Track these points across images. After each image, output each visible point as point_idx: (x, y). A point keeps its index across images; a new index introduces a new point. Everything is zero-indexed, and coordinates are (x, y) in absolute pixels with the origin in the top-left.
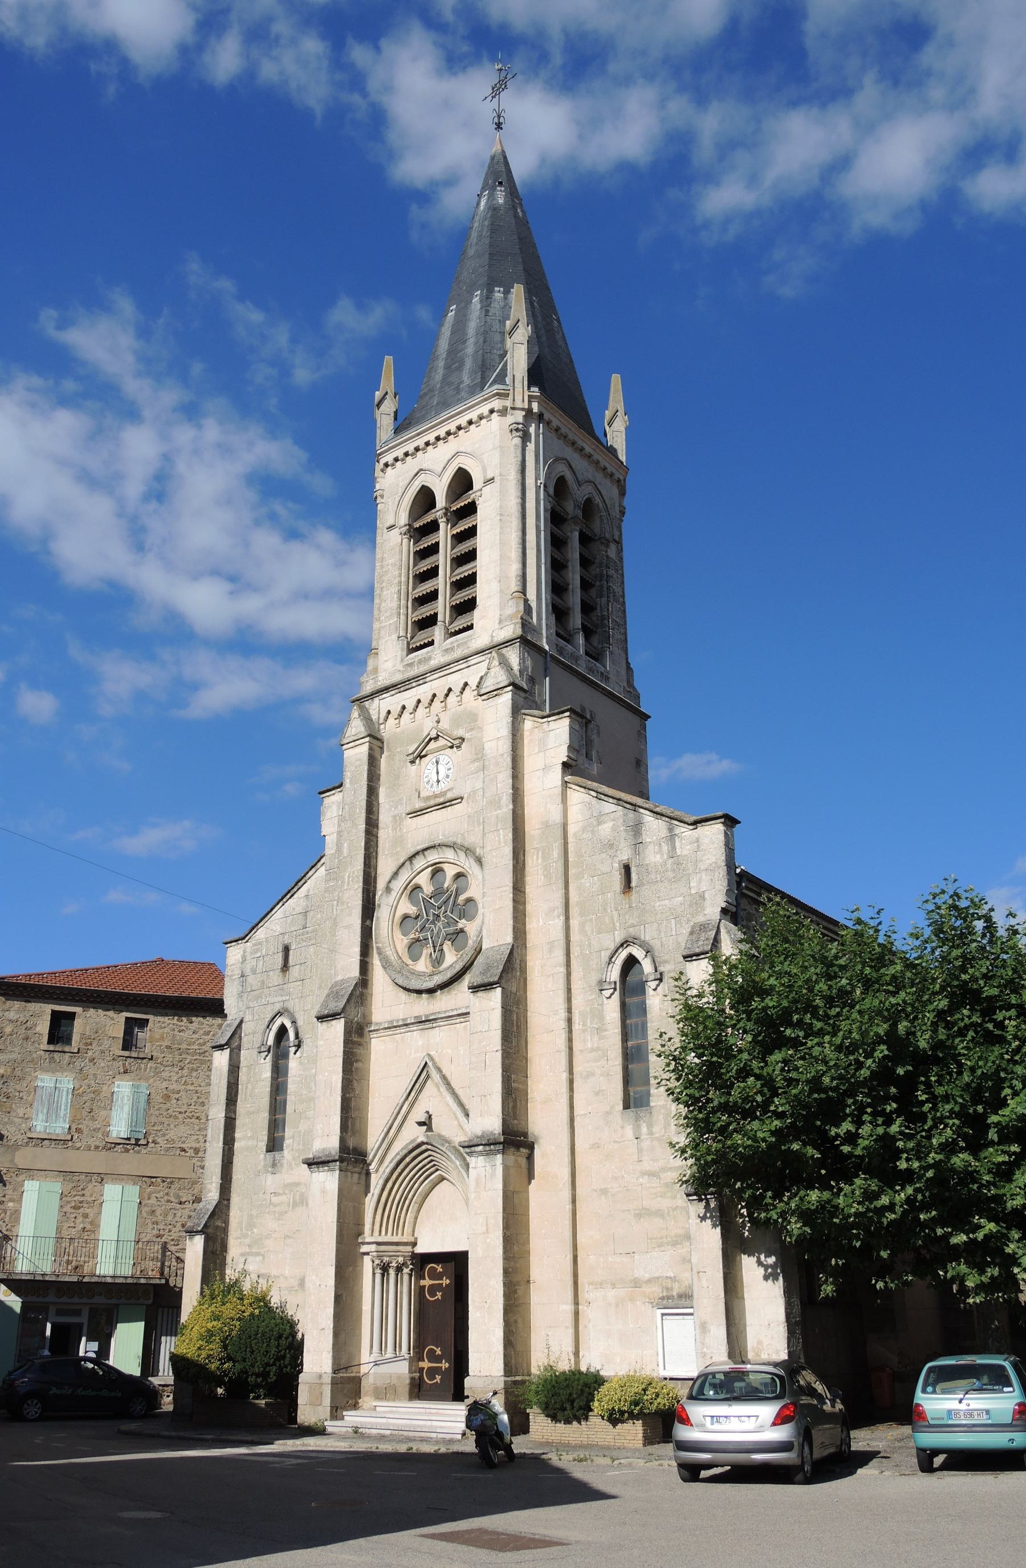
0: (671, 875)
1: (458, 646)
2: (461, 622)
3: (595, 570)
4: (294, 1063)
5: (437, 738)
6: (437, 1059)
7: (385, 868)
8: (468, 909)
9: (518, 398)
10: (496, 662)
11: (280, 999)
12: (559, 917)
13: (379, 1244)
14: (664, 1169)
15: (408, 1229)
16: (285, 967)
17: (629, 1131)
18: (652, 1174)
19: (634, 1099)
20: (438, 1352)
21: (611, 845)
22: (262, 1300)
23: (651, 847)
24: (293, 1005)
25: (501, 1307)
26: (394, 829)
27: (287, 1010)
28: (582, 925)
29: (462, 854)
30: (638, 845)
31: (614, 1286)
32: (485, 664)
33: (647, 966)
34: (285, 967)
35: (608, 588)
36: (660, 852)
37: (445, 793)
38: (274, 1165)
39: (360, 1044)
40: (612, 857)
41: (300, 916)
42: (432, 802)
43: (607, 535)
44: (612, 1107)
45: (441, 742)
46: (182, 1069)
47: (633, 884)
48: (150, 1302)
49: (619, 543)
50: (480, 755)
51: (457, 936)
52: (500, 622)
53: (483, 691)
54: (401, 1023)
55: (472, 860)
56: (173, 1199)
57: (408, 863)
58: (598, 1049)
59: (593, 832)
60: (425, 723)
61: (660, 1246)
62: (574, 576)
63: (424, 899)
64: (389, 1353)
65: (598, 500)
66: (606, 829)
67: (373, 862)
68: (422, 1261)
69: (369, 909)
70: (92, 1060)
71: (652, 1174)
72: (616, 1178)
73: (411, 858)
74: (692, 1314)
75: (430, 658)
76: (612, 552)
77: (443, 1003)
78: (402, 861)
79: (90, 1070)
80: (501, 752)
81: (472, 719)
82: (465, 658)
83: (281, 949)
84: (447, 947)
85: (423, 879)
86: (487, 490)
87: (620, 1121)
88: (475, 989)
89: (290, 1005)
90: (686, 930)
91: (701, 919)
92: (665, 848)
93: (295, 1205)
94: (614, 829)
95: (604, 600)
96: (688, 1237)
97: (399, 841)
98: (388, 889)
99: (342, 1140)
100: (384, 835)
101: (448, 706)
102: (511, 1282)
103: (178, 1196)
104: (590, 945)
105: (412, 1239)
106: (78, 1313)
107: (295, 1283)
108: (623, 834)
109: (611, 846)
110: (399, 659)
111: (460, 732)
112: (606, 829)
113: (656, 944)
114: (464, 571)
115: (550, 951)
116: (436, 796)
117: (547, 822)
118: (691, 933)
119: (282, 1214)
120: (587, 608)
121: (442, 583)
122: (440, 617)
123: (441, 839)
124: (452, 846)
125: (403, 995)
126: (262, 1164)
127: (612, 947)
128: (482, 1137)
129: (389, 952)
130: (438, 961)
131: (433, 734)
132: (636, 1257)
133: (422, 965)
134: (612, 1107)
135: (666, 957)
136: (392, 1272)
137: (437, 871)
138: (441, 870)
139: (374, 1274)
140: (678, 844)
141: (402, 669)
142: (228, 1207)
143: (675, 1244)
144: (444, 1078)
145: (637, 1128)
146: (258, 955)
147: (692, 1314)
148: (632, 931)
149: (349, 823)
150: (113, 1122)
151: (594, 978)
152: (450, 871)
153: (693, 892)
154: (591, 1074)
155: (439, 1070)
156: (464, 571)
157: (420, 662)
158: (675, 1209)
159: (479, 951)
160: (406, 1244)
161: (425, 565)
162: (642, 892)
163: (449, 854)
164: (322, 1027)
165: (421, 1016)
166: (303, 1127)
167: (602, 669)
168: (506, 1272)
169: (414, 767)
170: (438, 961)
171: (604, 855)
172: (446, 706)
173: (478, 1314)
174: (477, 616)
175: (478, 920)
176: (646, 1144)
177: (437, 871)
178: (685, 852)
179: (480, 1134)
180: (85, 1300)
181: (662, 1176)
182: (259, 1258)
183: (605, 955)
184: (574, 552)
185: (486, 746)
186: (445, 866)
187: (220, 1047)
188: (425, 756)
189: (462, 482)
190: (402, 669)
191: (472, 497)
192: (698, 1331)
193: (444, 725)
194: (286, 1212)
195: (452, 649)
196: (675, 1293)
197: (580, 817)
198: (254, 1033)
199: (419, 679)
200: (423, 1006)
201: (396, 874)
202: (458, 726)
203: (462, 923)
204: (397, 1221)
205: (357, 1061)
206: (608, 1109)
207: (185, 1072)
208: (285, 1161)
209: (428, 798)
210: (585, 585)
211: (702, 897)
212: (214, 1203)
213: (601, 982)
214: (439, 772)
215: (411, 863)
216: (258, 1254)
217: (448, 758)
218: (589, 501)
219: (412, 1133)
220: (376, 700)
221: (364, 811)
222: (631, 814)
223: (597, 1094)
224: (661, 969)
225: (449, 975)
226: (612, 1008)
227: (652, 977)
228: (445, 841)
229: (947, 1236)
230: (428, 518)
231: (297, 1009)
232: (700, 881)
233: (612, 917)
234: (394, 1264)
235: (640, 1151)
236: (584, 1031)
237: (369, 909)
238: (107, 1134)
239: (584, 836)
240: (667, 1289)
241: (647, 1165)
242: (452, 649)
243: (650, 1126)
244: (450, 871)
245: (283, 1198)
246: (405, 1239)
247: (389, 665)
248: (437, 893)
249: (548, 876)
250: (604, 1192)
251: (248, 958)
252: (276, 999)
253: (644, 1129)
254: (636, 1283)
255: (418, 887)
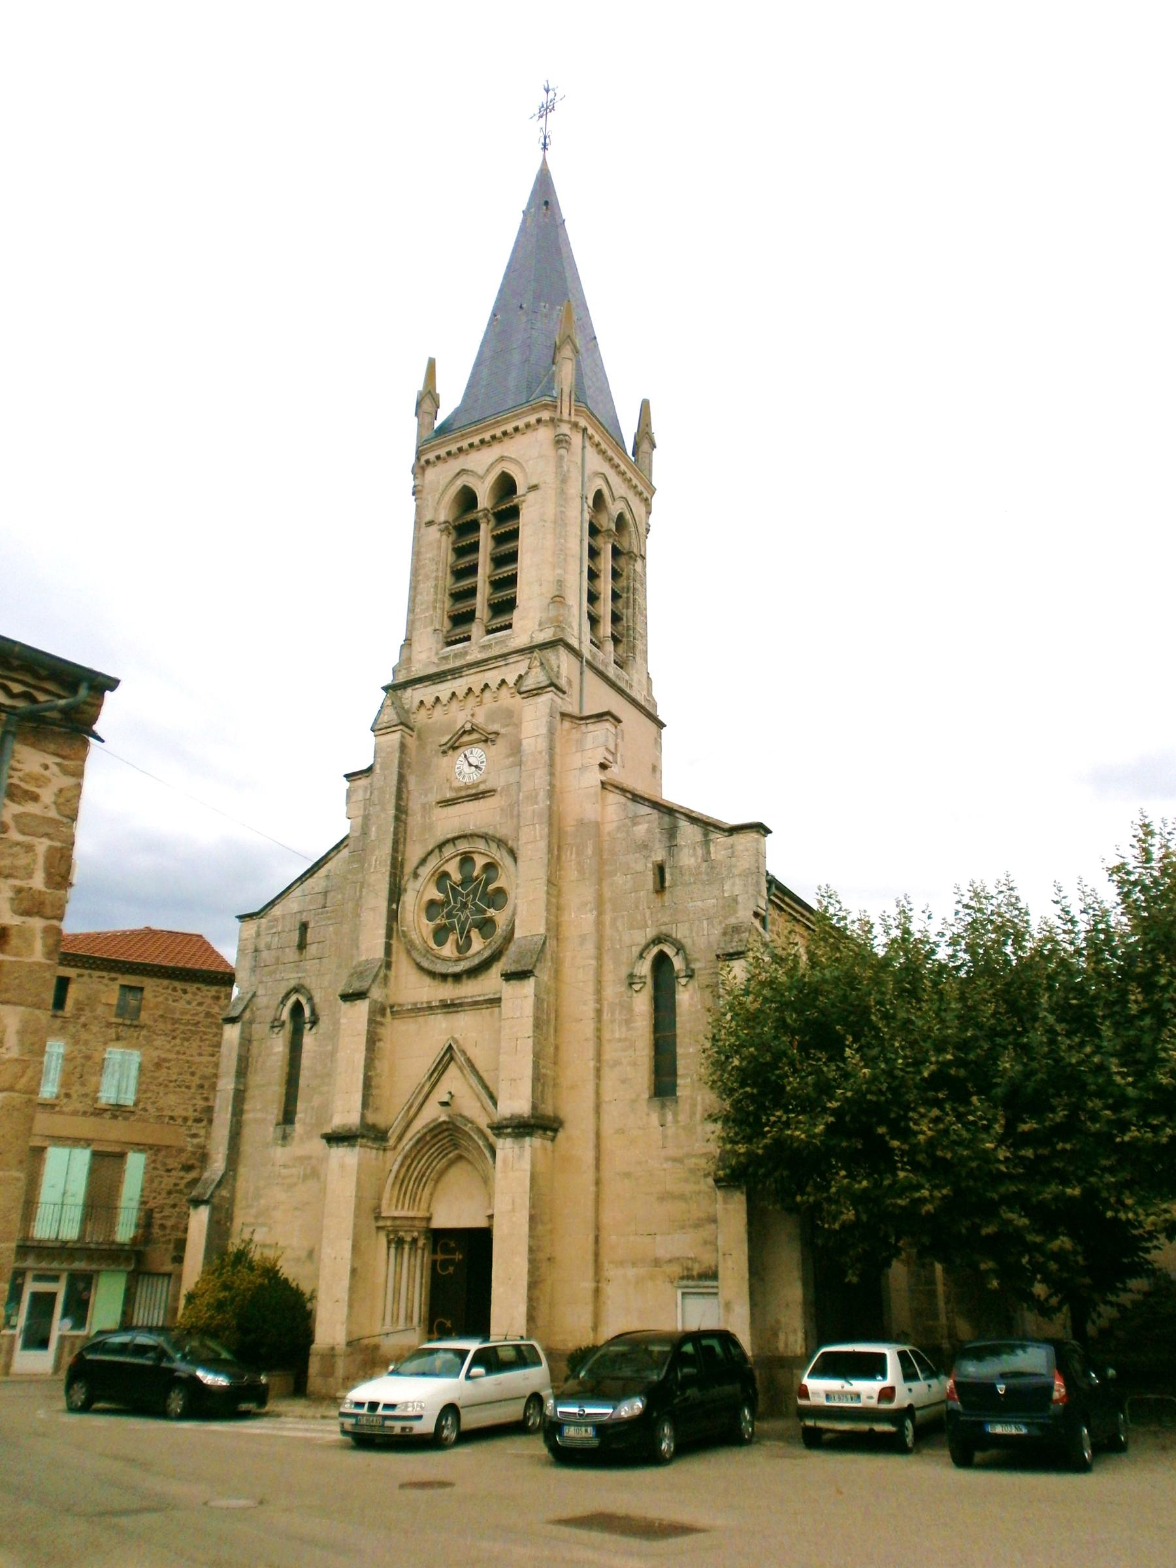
0: (705, 877)
1: (496, 643)
2: (501, 620)
3: (623, 582)
4: (309, 1040)
5: (470, 732)
6: (461, 1042)
7: (414, 852)
8: (498, 898)
9: (566, 411)
10: (537, 663)
11: (296, 975)
12: (591, 911)
13: (394, 1218)
14: (689, 1155)
15: (424, 1205)
16: (302, 946)
17: (655, 1119)
18: (675, 1160)
19: (663, 1085)
20: (449, 1324)
21: (645, 846)
22: (271, 1273)
23: (686, 850)
24: (310, 982)
25: (525, 1283)
26: (423, 816)
27: (302, 986)
28: (614, 920)
29: (494, 846)
30: (672, 846)
31: (634, 1264)
32: (528, 661)
33: (678, 963)
34: (302, 946)
35: (634, 600)
36: (695, 855)
37: (478, 785)
38: (285, 1137)
39: (382, 1024)
40: (647, 857)
41: (320, 896)
42: (463, 793)
43: (635, 551)
44: (638, 1096)
45: (475, 736)
46: (174, 1038)
47: (667, 884)
48: (132, 1267)
49: (643, 558)
50: (516, 749)
51: (486, 926)
52: (540, 625)
53: (524, 689)
54: (425, 1005)
55: (505, 854)
56: (159, 1166)
57: (437, 851)
58: (625, 1039)
59: (627, 832)
60: (460, 717)
61: (683, 1228)
62: (605, 586)
63: (452, 888)
64: (401, 1325)
65: (628, 516)
66: (641, 830)
67: (401, 847)
68: (440, 1238)
69: (396, 893)
70: (84, 1025)
71: (675, 1160)
72: (640, 1163)
73: (441, 847)
74: (716, 1294)
75: (466, 653)
76: (638, 566)
77: (470, 989)
78: (430, 848)
79: (84, 1036)
80: (539, 749)
81: (510, 717)
82: (504, 656)
83: (298, 926)
84: (475, 934)
85: (452, 868)
86: (531, 496)
87: (645, 1109)
88: (508, 977)
89: (307, 982)
90: (717, 931)
91: (733, 921)
92: (700, 852)
93: (305, 1178)
94: (649, 831)
95: (631, 610)
96: (713, 1220)
97: (428, 828)
98: (416, 875)
99: (363, 1116)
100: (415, 820)
101: (484, 701)
102: (535, 1260)
103: (165, 1164)
104: (620, 940)
105: (428, 1215)
106: (55, 1279)
107: (304, 1254)
108: (659, 836)
109: (646, 847)
110: (434, 650)
111: (495, 727)
112: (641, 830)
113: (687, 942)
114: (505, 571)
115: (582, 944)
116: (468, 788)
117: (582, 820)
118: (725, 934)
119: (291, 1186)
120: (616, 618)
121: (482, 580)
122: (477, 614)
123: (471, 829)
124: (484, 837)
125: (427, 980)
126: (271, 1136)
127: (643, 942)
128: (512, 1118)
129: (414, 936)
130: (463, 947)
131: (468, 727)
132: (658, 1238)
133: (448, 950)
134: (638, 1096)
135: (696, 956)
136: (407, 1247)
137: (466, 860)
138: (472, 859)
139: (389, 1248)
140: (712, 849)
141: (436, 661)
142: (235, 1178)
143: (697, 1226)
144: (468, 1060)
145: (662, 1116)
146: (274, 931)
147: (716, 1294)
148: (664, 929)
149: (378, 808)
150: (104, 1087)
151: (624, 972)
152: (480, 861)
153: (726, 895)
154: (617, 1063)
155: (464, 1052)
156: (505, 571)
157: (456, 656)
158: (699, 1193)
159: (509, 937)
160: (421, 1219)
161: (464, 562)
162: (676, 894)
163: (481, 845)
164: (345, 1006)
165: (446, 1000)
166: (317, 1101)
167: (627, 677)
168: (531, 1250)
169: (445, 759)
170: (463, 947)
171: (637, 855)
172: (481, 702)
173: (501, 1290)
174: (516, 616)
175: (508, 909)
176: (671, 1130)
177: (466, 860)
178: (719, 857)
179: (508, 1116)
180: (65, 1266)
181: (686, 1161)
182: (265, 1229)
183: (636, 951)
184: (606, 563)
185: (525, 742)
186: (476, 857)
187: (232, 1020)
188: (457, 748)
189: (506, 486)
190: (436, 661)
191: (516, 501)
192: (722, 1311)
193: (480, 720)
194: (295, 1185)
195: (490, 646)
196: (695, 1273)
197: (615, 818)
198: (267, 1007)
199: (455, 673)
200: (447, 992)
201: (423, 861)
202: (493, 722)
203: (491, 912)
204: (413, 1198)
205: (380, 1040)
206: (633, 1096)
207: (178, 1041)
208: (296, 1134)
209: (460, 789)
210: (615, 596)
211: (735, 900)
212: (220, 1173)
213: (631, 976)
214: (468, 766)
215: (440, 851)
216: (264, 1225)
217: (477, 754)
218: (621, 517)
219: (432, 1113)
220: (409, 690)
221: (393, 797)
222: (667, 819)
223: (623, 1082)
224: (692, 966)
225: (476, 961)
226: (642, 1003)
227: (683, 974)
228: (477, 831)
229: (975, 1229)
230: (470, 517)
231: (313, 986)
232: (733, 884)
233: (644, 915)
234: (409, 1239)
235: (665, 1137)
236: (613, 1021)
237: (396, 893)
238: (96, 1100)
239: (619, 835)
240: (688, 1269)
241: (672, 1152)
242: (490, 646)
243: (675, 1114)
244: (480, 861)
245: (294, 1171)
246: (421, 1214)
247: (423, 656)
248: (466, 881)
249: (581, 871)
250: (628, 1175)
251: (263, 933)
252: (292, 975)
253: (670, 1117)
254: (657, 1262)
255: (445, 875)
